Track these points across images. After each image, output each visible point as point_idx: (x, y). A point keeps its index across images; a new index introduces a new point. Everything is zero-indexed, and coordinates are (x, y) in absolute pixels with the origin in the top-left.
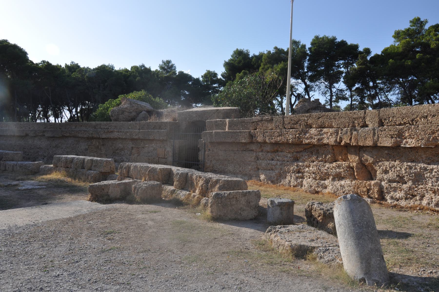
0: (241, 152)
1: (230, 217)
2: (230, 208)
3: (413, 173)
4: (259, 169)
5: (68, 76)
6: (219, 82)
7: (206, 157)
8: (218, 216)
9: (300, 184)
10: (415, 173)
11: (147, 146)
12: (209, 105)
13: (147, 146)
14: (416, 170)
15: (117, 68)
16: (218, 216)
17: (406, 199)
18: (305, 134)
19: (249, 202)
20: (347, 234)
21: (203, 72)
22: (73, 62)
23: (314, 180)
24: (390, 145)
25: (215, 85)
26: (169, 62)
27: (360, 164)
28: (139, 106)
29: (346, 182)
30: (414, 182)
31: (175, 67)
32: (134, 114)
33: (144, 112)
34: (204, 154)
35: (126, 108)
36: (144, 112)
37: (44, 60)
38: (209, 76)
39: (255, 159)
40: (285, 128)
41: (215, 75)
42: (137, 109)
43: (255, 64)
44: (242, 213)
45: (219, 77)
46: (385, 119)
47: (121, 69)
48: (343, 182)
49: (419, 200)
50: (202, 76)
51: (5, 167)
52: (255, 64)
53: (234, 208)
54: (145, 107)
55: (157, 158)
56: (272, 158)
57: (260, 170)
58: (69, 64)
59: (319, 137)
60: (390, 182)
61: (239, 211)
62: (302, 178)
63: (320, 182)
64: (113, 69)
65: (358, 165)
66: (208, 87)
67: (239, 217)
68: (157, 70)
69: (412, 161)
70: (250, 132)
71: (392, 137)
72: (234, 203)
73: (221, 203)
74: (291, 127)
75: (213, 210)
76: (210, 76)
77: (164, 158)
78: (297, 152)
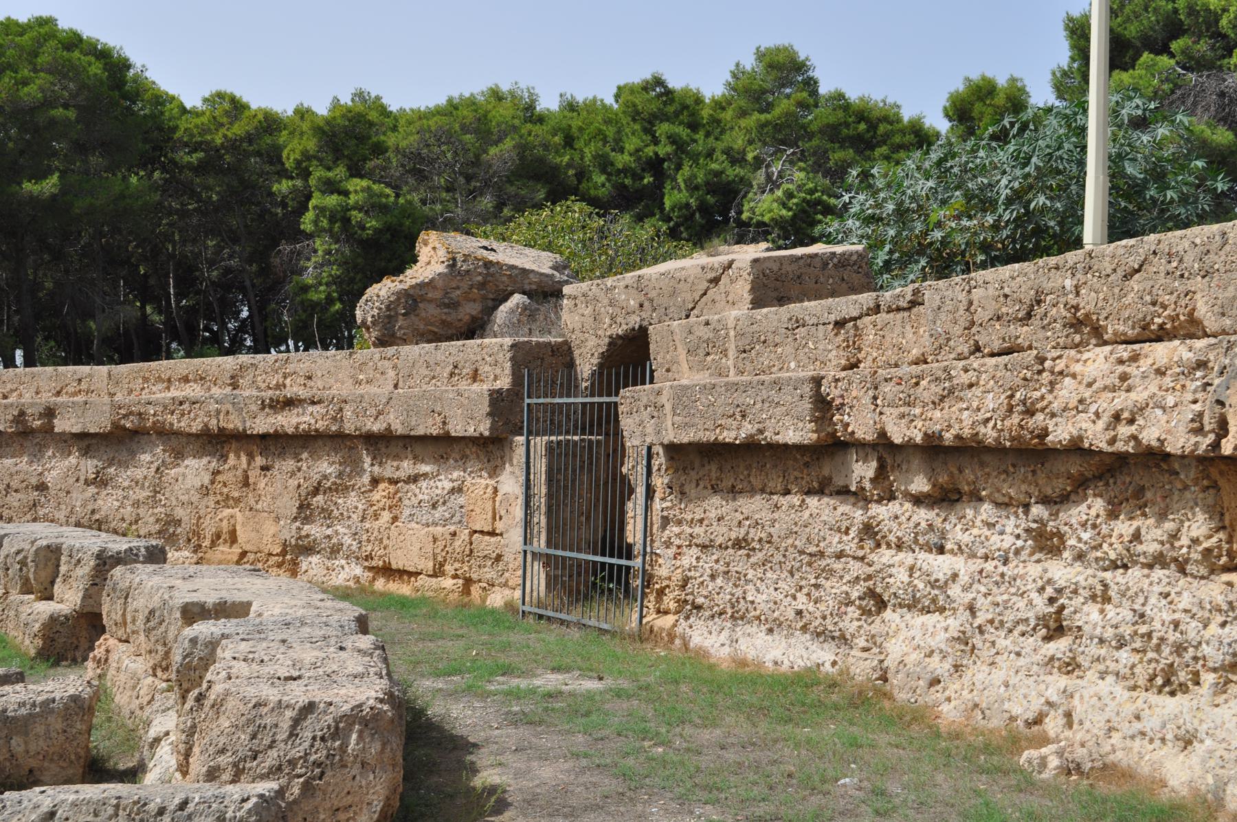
77: (492, 533)
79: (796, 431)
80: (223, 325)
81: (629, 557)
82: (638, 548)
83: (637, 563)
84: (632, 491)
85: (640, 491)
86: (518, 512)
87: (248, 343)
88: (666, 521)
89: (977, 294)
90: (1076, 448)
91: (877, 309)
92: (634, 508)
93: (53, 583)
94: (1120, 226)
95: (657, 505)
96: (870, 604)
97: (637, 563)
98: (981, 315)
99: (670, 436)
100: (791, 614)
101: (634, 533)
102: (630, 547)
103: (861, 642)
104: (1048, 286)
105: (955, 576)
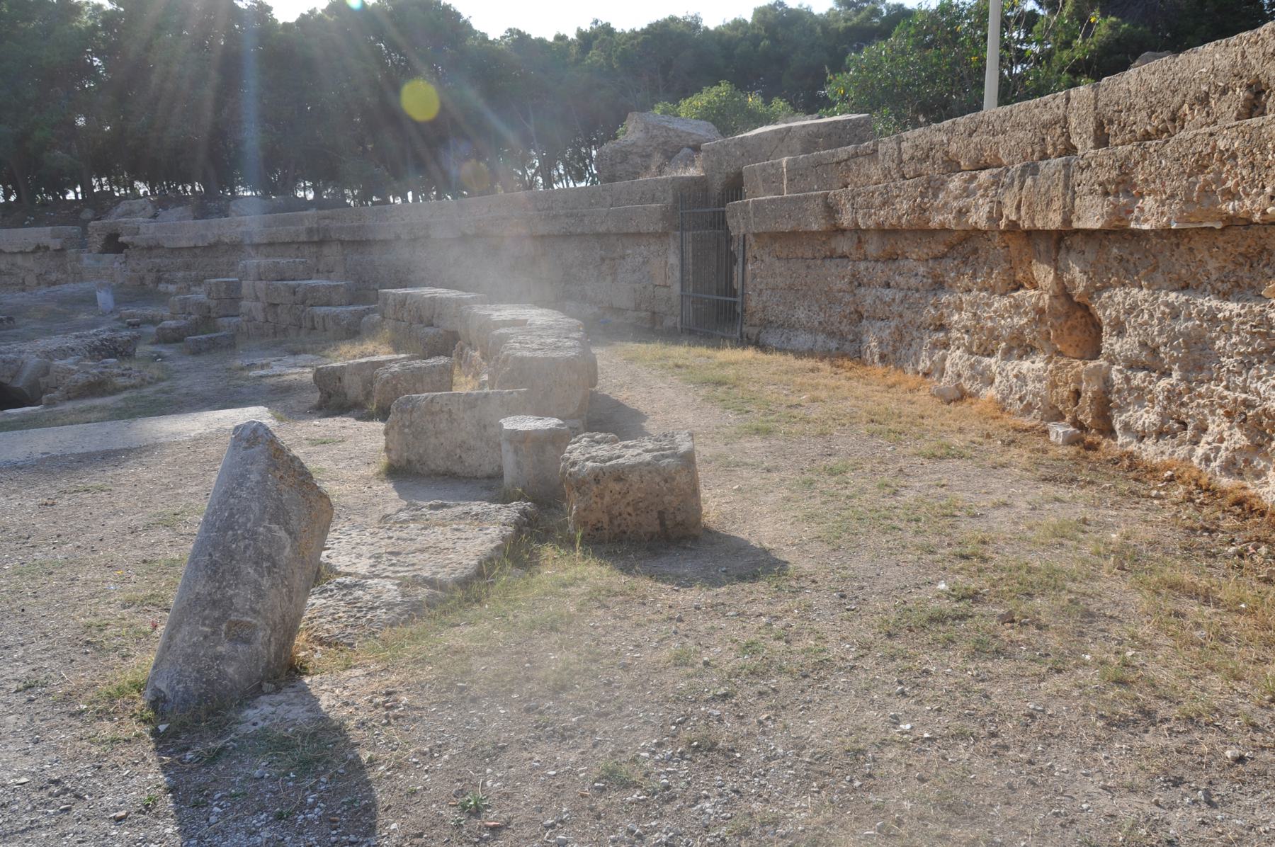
0: (819, 262)
1: (433, 466)
2: (433, 440)
3: (1181, 334)
4: (861, 317)
7: (749, 280)
8: (404, 463)
9: (939, 367)
10: (1186, 335)
11: (629, 252)
12: (808, 113)
13: (629, 252)
14: (1190, 324)
15: (712, 20)
16: (404, 463)
17: (1160, 434)
18: (935, 196)
19: (485, 427)
20: (493, 546)
22: (596, 22)
23: (966, 356)
24: (1098, 226)
27: (1063, 300)
28: (671, 133)
29: (1033, 366)
30: (1187, 371)
34: (744, 270)
35: (633, 144)
37: (512, 27)
39: (851, 283)
40: (904, 177)
42: (665, 143)
44: (464, 456)
46: (1111, 122)
48: (1026, 365)
49: (1190, 440)
51: (313, 321)
53: (443, 440)
54: (689, 134)
55: (651, 288)
56: (885, 279)
57: (864, 322)
58: (586, 27)
59: (961, 203)
60: (1131, 368)
61: (458, 451)
62: (946, 346)
63: (979, 362)
64: (697, 26)
65: (1057, 304)
67: (457, 468)
68: (831, 9)
69: (1185, 288)
70: (826, 196)
71: (1106, 194)
72: (443, 426)
73: (409, 427)
74: (915, 171)
75: (391, 446)
77: (665, 286)
78: (935, 258)
79: (816, 224)
80: (525, 172)
81: (735, 296)
82: (739, 292)
83: (739, 299)
84: (736, 261)
85: (740, 260)
86: (678, 274)
87: (162, 728)
88: (754, 276)
89: (904, 145)
90: (943, 230)
91: (856, 155)
92: (737, 270)
93: (1144, 369)
94: (1008, 94)
95: (749, 267)
96: (855, 316)
97: (739, 299)
98: (905, 157)
99: (753, 229)
100: (816, 323)
101: (737, 284)
102: (735, 291)
103: (850, 337)
104: (935, 139)
105: (894, 300)
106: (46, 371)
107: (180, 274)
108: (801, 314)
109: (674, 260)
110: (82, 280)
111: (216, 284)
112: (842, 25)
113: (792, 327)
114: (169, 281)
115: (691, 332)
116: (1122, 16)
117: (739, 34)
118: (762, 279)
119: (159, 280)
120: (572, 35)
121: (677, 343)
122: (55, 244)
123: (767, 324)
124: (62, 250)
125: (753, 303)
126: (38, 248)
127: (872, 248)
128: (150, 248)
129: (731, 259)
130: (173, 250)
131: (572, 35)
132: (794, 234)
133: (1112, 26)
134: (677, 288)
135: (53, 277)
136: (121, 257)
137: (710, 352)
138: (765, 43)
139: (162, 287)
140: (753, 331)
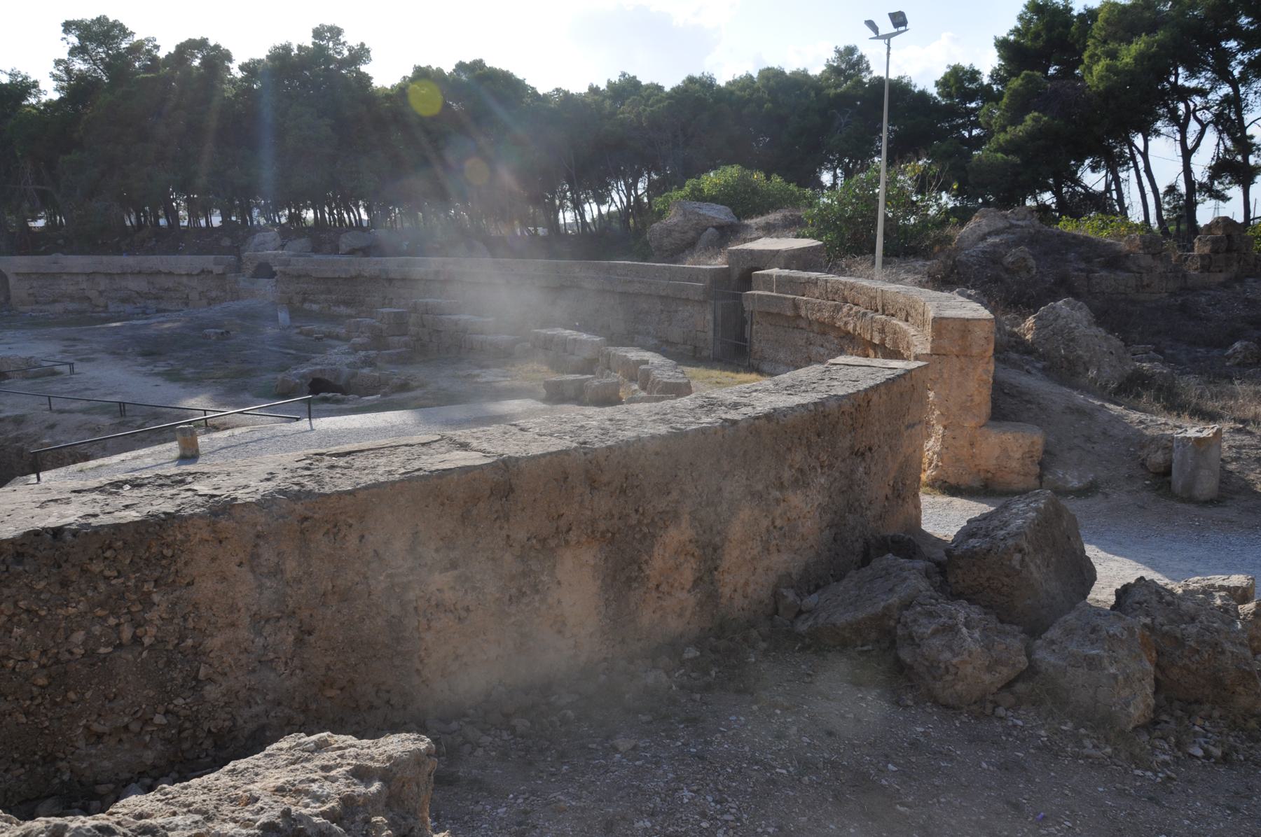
5: (613, 114)
6: (985, 93)
21: (940, 72)
25: (973, 105)
26: (850, 51)
31: (867, 63)
32: (692, 234)
33: (711, 229)
35: (676, 225)
36: (711, 229)
38: (952, 81)
41: (974, 75)
43: (1078, 41)
45: (986, 80)
47: (737, 77)
50: (937, 84)
52: (1078, 41)
58: (615, 78)
59: (191, 468)
66: (949, 112)
76: (959, 81)
86: (712, 325)
92: (747, 328)
101: (747, 335)
106: (354, 375)
107: (323, 297)
108: (781, 355)
109: (709, 317)
110: (238, 298)
111: (389, 314)
112: (832, 91)
113: (777, 362)
114: (312, 301)
115: (719, 361)
116: (1043, 112)
117: (746, 94)
118: (760, 336)
119: (304, 300)
120: (603, 86)
121: (713, 368)
122: (218, 270)
123: (763, 359)
124: (224, 274)
125: (756, 347)
126: (203, 271)
127: (816, 328)
128: (299, 276)
129: (744, 322)
130: (318, 279)
131: (603, 86)
132: (778, 314)
133: (1034, 119)
134: (711, 333)
135: (214, 294)
136: (272, 281)
137: (732, 375)
138: (768, 105)
139: (306, 306)
140: (756, 362)
